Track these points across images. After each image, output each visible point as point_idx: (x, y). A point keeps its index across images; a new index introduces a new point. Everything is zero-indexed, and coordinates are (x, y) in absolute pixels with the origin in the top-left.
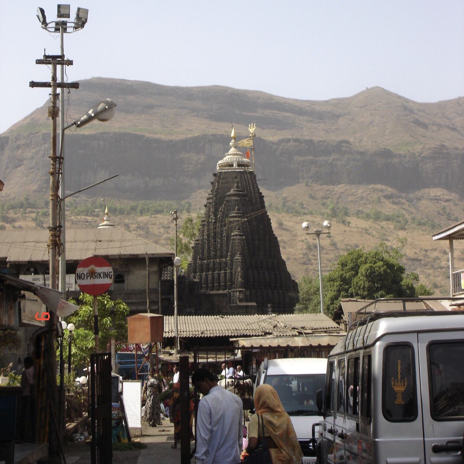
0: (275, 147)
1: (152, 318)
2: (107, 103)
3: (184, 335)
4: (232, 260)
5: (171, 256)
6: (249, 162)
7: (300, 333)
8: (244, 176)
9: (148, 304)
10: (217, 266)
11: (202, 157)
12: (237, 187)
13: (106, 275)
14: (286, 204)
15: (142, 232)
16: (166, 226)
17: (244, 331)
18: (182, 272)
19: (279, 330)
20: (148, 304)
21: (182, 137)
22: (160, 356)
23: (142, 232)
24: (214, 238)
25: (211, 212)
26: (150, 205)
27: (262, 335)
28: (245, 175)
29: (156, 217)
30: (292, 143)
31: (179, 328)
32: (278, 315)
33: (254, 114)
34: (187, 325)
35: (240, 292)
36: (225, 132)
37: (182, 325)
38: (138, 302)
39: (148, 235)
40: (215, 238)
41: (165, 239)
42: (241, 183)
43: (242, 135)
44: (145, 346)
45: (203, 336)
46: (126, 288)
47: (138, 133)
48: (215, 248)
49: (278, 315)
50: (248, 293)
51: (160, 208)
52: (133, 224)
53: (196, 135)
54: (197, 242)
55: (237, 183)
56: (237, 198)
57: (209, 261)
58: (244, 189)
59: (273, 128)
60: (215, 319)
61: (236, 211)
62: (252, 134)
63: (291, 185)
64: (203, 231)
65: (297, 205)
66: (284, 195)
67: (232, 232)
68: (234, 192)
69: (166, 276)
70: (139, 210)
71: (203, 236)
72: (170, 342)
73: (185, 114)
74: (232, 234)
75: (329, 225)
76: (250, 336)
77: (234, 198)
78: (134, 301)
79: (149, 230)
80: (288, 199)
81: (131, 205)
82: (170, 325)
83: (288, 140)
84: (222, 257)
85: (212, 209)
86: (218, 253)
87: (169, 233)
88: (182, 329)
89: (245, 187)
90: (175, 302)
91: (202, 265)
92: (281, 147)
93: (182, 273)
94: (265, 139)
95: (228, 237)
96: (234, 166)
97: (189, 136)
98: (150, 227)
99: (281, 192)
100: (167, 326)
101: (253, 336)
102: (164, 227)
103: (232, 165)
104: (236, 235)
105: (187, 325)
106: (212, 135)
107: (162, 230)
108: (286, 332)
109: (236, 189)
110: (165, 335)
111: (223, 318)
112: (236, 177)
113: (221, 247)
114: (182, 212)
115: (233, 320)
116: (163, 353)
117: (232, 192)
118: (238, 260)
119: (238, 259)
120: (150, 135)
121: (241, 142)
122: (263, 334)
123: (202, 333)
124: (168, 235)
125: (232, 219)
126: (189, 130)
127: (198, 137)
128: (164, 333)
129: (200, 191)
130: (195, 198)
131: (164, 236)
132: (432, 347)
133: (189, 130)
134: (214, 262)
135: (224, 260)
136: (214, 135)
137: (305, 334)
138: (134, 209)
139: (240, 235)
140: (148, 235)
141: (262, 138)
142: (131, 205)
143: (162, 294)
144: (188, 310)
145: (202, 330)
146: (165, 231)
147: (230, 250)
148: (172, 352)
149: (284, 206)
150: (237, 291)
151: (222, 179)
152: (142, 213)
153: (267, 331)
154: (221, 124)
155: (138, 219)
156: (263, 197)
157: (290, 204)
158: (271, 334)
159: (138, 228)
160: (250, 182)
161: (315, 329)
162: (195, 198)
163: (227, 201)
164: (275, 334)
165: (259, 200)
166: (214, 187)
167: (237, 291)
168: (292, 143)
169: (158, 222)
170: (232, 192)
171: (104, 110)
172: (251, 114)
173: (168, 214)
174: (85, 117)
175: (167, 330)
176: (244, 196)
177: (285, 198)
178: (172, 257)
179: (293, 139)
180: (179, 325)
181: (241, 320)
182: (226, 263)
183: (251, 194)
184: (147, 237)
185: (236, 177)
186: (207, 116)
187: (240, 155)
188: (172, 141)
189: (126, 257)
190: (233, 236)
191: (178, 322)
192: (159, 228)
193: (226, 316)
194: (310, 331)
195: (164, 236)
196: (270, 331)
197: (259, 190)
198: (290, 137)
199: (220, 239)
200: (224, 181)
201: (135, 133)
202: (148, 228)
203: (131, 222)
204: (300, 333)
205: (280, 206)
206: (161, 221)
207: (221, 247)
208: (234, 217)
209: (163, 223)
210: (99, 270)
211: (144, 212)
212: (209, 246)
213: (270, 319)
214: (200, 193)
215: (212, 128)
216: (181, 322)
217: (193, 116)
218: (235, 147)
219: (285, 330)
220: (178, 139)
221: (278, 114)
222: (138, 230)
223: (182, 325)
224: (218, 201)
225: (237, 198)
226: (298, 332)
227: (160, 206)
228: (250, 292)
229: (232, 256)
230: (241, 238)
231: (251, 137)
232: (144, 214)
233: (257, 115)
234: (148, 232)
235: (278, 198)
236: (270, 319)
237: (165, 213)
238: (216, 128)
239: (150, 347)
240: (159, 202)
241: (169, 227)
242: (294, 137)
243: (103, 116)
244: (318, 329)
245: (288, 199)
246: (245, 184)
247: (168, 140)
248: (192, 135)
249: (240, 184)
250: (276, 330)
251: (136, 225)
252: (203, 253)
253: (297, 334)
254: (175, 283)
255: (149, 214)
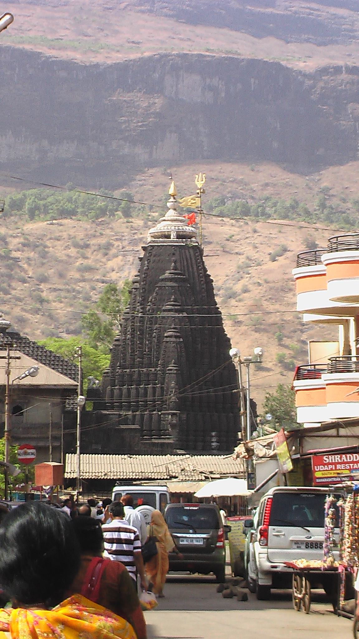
0: (308, 83)
1: (54, 466)
2: (35, 368)
3: (86, 476)
4: (164, 373)
5: (75, 388)
6: (193, 232)
7: (207, 478)
8: (185, 252)
9: (51, 450)
10: (143, 378)
11: (159, 102)
12: (175, 269)
13: (32, 454)
14: (328, 203)
15: (32, 255)
16: (81, 243)
17: (150, 474)
18: (94, 383)
19: (186, 474)
20: (51, 450)
21: (118, 58)
22: (60, 497)
23: (32, 255)
24: (141, 339)
25: (137, 301)
26: (50, 199)
27: (167, 479)
28: (187, 251)
29: (61, 225)
30: (344, 76)
31: (81, 469)
32: (192, 456)
33: (269, 10)
34: (91, 465)
35: (173, 414)
36: (208, 50)
37: (85, 465)
38: (37, 438)
39: (45, 261)
40: (142, 339)
41: (79, 270)
42: (181, 263)
43: (243, 57)
44: (48, 487)
45: (106, 477)
46: (25, 421)
47: (28, 47)
48: (142, 352)
49: (192, 456)
50: (184, 416)
51: (69, 206)
52: (14, 237)
53: (147, 54)
54: (117, 343)
55: (175, 262)
56: (174, 284)
57: (133, 370)
58: (184, 271)
59: (307, 41)
60: (122, 459)
61: (172, 303)
62: (200, 189)
63: (341, 163)
64: (126, 327)
65: (349, 205)
66: (324, 184)
67: (165, 331)
68: (170, 276)
69: (69, 408)
70: (27, 207)
71: (125, 334)
72: (72, 483)
73: (126, 7)
74: (165, 335)
75: (260, 353)
76: (154, 479)
77: (169, 284)
78: (35, 436)
79: (46, 250)
80: (331, 192)
81: (11, 198)
82: (73, 464)
83: (338, 70)
84: (150, 365)
85: (138, 298)
86: (146, 361)
87: (87, 258)
88: (85, 469)
89: (186, 268)
90: (78, 442)
91: (122, 376)
92: (321, 84)
93: (94, 386)
94: (290, 66)
95: (160, 337)
96: (172, 237)
97: (133, 56)
98: (48, 243)
99: (318, 178)
100: (69, 465)
101: (157, 479)
102: (76, 245)
103: (168, 237)
104: (170, 336)
105: (91, 465)
106: (178, 55)
107: (73, 251)
108: (192, 476)
109: (173, 271)
110: (66, 476)
111: (131, 458)
112: (174, 254)
113: (150, 351)
114: (114, 215)
115: (141, 461)
116: (64, 494)
117: (167, 275)
118: (172, 372)
119: (171, 370)
120: (53, 53)
121: (184, 201)
122: (168, 477)
123: (105, 475)
124: (85, 262)
125: (165, 314)
126: (133, 42)
127: (150, 59)
128: (66, 474)
129: (151, 171)
130: (142, 185)
131: (78, 264)
132: (161, 494)
133: (133, 42)
134: (139, 371)
135: (153, 370)
136: (184, 56)
137: (212, 478)
138: (17, 205)
139: (176, 337)
140: (45, 261)
141: (283, 63)
142: (11, 198)
143: (64, 429)
144: (94, 447)
145: (106, 471)
146: (78, 252)
147: (162, 356)
148: (73, 494)
149: (323, 206)
150: (169, 414)
151: (155, 256)
152: (32, 215)
153: (174, 474)
154: (200, 30)
155: (25, 228)
156: (212, 281)
157: (334, 202)
158: (177, 477)
159: (24, 245)
160: (194, 261)
161: (224, 474)
162: (142, 185)
163: (160, 287)
164: (181, 477)
165: (204, 286)
166: (142, 265)
167: (169, 414)
168: (344, 76)
169: (65, 235)
170: (167, 275)
171: (34, 372)
172: (262, 10)
173: (85, 218)
174: (24, 375)
175: (69, 471)
176: (184, 280)
177: (325, 191)
178: (76, 389)
179: (347, 67)
180: (81, 465)
181: (156, 462)
182: (156, 374)
183: (194, 278)
184: (43, 264)
185: (174, 254)
186: (172, 13)
187: (181, 221)
188: (97, 66)
189: (26, 387)
190: (167, 337)
191: (81, 462)
192: (67, 247)
193: (134, 456)
194: (218, 476)
195: (78, 264)
196: (177, 475)
197: (206, 270)
198: (341, 63)
199: (148, 340)
200: (157, 259)
201: (21, 46)
202: (46, 247)
203: (11, 232)
204: (207, 478)
205: (313, 205)
206: (72, 232)
207: (150, 351)
208: (168, 311)
209: (75, 237)
210: (29, 451)
211: (37, 212)
212: (134, 349)
213: (181, 460)
214: (152, 175)
215: (181, 40)
216: (85, 461)
217: (143, 12)
218: (175, 209)
219: (192, 474)
220: (109, 62)
221: (318, 10)
222: (25, 248)
223: (85, 465)
224: (147, 287)
225: (174, 284)
226: (205, 477)
227: (70, 200)
228: (188, 414)
229: (164, 365)
230: (178, 340)
231: (198, 193)
232: (37, 218)
233: (275, 11)
234: (44, 255)
235: (310, 188)
236: (181, 460)
237: (79, 217)
238: (189, 40)
239: (51, 488)
240: (67, 194)
241: (87, 246)
242: (350, 64)
243: (33, 375)
244: (227, 473)
245: (331, 192)
246: (185, 264)
247: (88, 64)
248: (139, 55)
249: (178, 264)
250: (183, 473)
251: (22, 240)
252: (124, 359)
253: (204, 478)
254: (78, 423)
255: (48, 217)
